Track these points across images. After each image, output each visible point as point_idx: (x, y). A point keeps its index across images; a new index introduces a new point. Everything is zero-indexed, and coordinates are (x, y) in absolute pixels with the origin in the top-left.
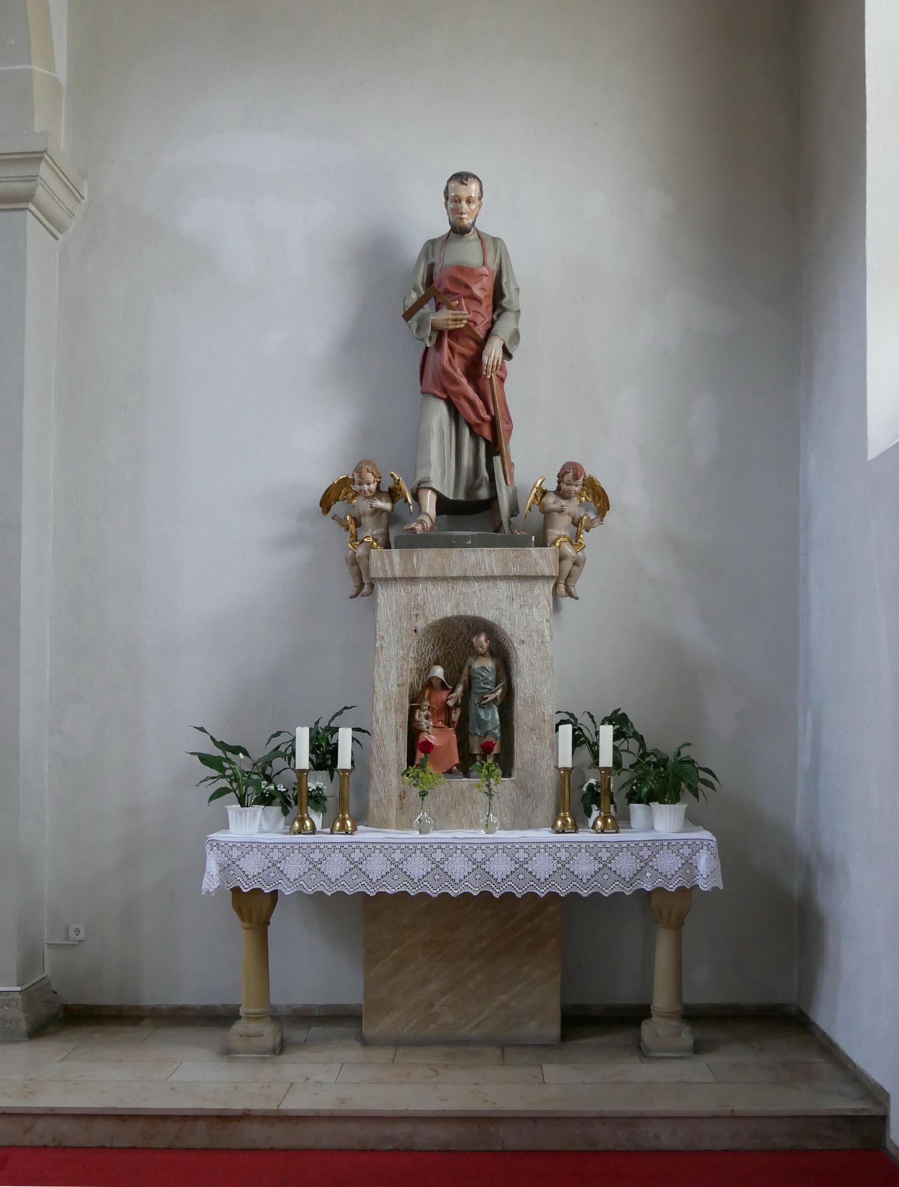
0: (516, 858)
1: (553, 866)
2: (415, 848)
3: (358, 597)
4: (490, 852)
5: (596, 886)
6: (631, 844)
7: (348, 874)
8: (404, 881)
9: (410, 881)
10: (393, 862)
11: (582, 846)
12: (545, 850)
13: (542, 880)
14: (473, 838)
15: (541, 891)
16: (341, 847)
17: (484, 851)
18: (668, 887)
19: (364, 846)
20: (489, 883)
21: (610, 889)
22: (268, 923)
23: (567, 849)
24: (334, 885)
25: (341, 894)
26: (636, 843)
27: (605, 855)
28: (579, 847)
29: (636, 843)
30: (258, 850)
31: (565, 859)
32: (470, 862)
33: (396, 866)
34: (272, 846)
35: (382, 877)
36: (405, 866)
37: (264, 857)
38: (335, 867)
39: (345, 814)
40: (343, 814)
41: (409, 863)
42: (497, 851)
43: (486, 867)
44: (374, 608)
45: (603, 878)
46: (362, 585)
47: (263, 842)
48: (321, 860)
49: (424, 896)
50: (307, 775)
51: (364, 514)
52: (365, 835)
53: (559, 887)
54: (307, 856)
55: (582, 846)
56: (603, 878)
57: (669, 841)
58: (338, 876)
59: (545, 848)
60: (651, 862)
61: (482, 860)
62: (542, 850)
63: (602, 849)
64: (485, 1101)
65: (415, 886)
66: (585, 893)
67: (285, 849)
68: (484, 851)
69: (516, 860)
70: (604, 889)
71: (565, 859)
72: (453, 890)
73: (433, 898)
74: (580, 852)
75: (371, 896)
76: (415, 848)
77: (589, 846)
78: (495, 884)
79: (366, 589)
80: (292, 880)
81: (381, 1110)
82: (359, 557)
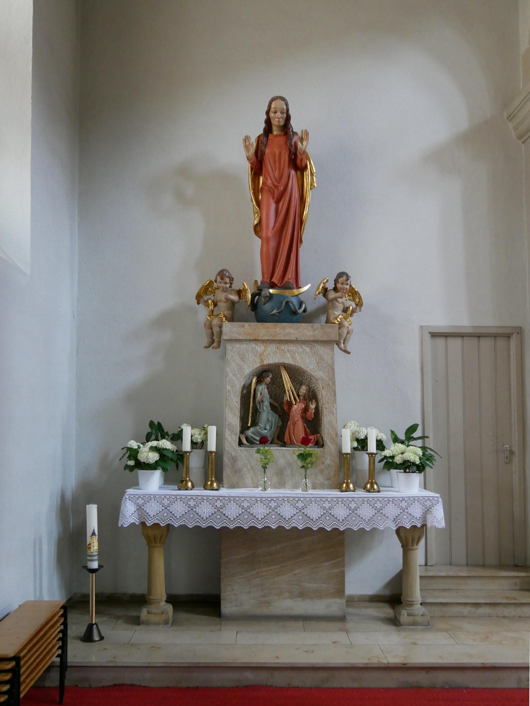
0: (297, 506)
1: (321, 512)
2: (337, 501)
3: (209, 348)
4: (226, 502)
5: (198, 522)
6: (131, 496)
7: (241, 515)
8: (197, 519)
9: (228, 520)
10: (401, 508)
11: (231, 499)
12: (367, 502)
13: (341, 521)
14: (319, 494)
15: (314, 526)
16: (342, 500)
17: (381, 502)
18: (148, 522)
19: (265, 499)
20: (171, 518)
21: (303, 525)
22: (402, 546)
23: (355, 502)
24: (261, 522)
25: (211, 528)
26: (134, 496)
27: (353, 505)
28: (229, 499)
29: (134, 496)
30: (261, 502)
31: (379, 508)
32: (322, 509)
33: (166, 508)
34: (216, 498)
35: (292, 517)
36: (333, 512)
37: (184, 504)
38: (205, 510)
39: (373, 480)
40: (347, 480)
41: (335, 509)
42: (389, 502)
43: (197, 510)
44: (223, 357)
45: (352, 519)
46: (213, 342)
47: (388, 497)
48: (303, 507)
49: (321, 530)
50: (189, 454)
51: (220, 301)
52: (224, 492)
53: (325, 524)
54: (373, 505)
55: (231, 499)
56: (326, 519)
57: (155, 496)
58: (181, 515)
59: (367, 501)
60: (248, 510)
61: (406, 507)
62: (366, 502)
63: (326, 502)
64: (17, 638)
65: (260, 522)
66: (260, 527)
67: (434, 500)
68: (381, 502)
69: (297, 507)
70: (244, 524)
71: (379, 508)
72: (229, 524)
73: (300, 530)
74: (177, 501)
75: (287, 529)
76: (337, 501)
77: (394, 500)
78: (180, 519)
79: (215, 344)
80: (178, 517)
81: (441, 663)
82: (214, 325)
